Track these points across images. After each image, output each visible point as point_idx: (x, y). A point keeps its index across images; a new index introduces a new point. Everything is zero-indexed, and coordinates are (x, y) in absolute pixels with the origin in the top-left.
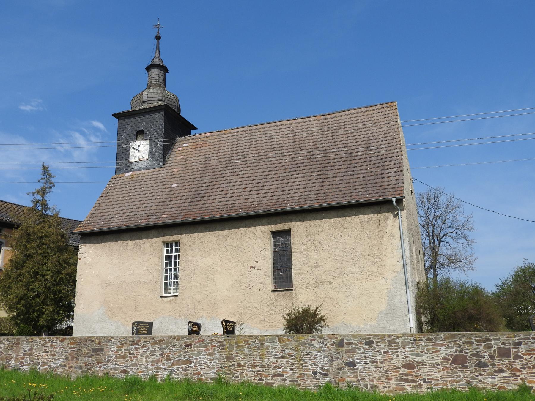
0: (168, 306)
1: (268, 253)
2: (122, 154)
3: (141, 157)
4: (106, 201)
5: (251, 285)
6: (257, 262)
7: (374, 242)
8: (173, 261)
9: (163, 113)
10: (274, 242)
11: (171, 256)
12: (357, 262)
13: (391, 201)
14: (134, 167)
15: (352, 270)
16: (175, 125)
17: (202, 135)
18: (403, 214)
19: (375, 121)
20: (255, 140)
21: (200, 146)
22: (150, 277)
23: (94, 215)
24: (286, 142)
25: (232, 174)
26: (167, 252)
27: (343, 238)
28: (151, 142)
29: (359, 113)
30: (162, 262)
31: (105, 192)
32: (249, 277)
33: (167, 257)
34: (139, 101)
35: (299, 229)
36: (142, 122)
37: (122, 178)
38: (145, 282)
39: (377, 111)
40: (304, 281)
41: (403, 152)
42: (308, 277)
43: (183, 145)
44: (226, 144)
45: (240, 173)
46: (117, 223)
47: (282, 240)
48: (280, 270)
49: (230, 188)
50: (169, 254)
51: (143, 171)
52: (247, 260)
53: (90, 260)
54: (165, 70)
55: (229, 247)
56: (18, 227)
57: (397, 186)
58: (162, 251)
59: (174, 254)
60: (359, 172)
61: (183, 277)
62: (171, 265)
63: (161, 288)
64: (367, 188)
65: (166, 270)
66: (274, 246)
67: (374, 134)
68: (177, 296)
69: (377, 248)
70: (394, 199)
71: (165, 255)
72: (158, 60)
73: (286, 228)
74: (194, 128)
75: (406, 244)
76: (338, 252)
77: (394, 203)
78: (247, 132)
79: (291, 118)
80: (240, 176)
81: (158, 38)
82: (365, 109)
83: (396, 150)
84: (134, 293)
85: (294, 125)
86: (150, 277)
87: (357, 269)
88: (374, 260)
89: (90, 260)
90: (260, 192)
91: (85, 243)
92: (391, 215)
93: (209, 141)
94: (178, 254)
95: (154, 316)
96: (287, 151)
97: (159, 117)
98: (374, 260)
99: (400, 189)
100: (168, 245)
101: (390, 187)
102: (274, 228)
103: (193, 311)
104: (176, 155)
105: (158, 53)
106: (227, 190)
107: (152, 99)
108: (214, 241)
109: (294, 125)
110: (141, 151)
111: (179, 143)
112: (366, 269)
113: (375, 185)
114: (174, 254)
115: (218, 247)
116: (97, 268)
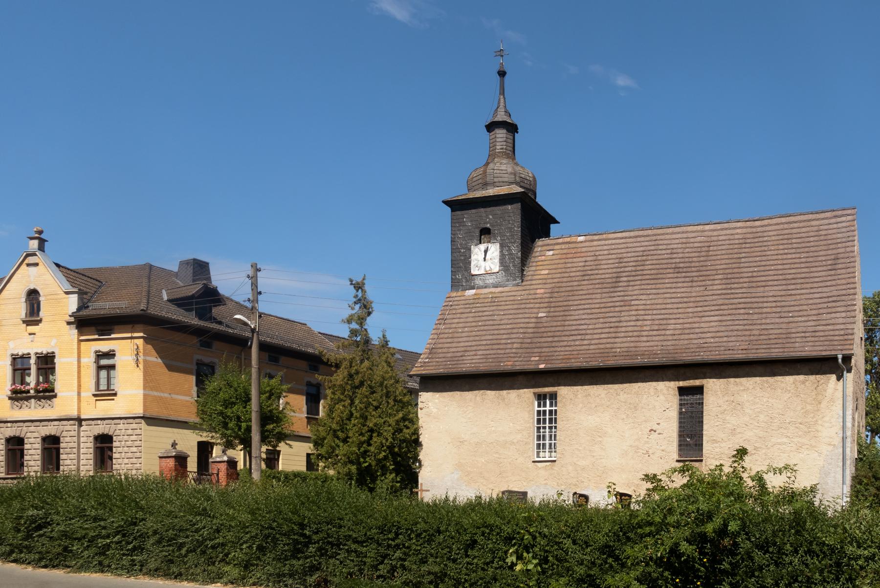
0: (542, 472)
1: (673, 415)
2: (460, 263)
3: (488, 269)
4: (447, 331)
5: (650, 452)
6: (658, 424)
7: (809, 407)
8: (547, 417)
9: (519, 205)
10: (681, 400)
11: (545, 412)
12: (785, 431)
13: (836, 358)
14: (478, 282)
15: (779, 441)
16: (536, 223)
17: (573, 239)
18: (849, 377)
19: (822, 238)
20: (652, 252)
21: (571, 256)
22: (519, 436)
23: (434, 351)
24: (695, 259)
25: (622, 303)
26: (539, 406)
27: (770, 400)
28: (502, 246)
29: (800, 222)
30: (533, 418)
31: (441, 317)
32: (647, 442)
33: (539, 412)
34: (480, 181)
35: (713, 387)
36: (488, 217)
37: (463, 298)
38: (512, 443)
39: (826, 221)
40: (717, 450)
41: (857, 285)
42: (722, 445)
43: (545, 252)
44: (610, 257)
45: (633, 302)
46: (470, 364)
47: (691, 397)
48: (688, 436)
49: (621, 324)
50: (542, 409)
51: (493, 290)
52: (645, 421)
53: (435, 410)
54: (512, 128)
55: (623, 404)
56: (337, 366)
57: (846, 337)
58: (533, 404)
59: (548, 408)
60: (796, 314)
61: (562, 438)
62: (544, 422)
63: (533, 450)
64: (805, 337)
65: (539, 428)
66: (681, 405)
67: (820, 259)
68: (555, 461)
69: (812, 415)
70: (840, 357)
71: (537, 409)
72: (503, 113)
73: (697, 382)
74: (555, 222)
75: (849, 412)
76: (762, 417)
77: (840, 361)
78: (639, 239)
79: (702, 222)
80: (634, 308)
81: (502, 74)
82: (811, 217)
83: (848, 286)
84: (497, 455)
85: (706, 233)
86: (519, 436)
87: (785, 440)
88: (806, 429)
89: (435, 410)
90: (663, 332)
91: (427, 390)
92: (834, 377)
93: (584, 250)
94: (554, 408)
95: (525, 484)
96: (771, 332)
97: (513, 211)
98: (806, 429)
99: (849, 342)
100: (541, 398)
101: (837, 338)
102: (682, 384)
103: (575, 480)
104: (538, 268)
105: (502, 100)
106: (617, 327)
107: (500, 179)
108: (603, 395)
109: (706, 233)
110: (486, 259)
111: (540, 249)
112: (796, 440)
113: (817, 334)
114: (548, 408)
115: (608, 403)
116: (441, 419)
